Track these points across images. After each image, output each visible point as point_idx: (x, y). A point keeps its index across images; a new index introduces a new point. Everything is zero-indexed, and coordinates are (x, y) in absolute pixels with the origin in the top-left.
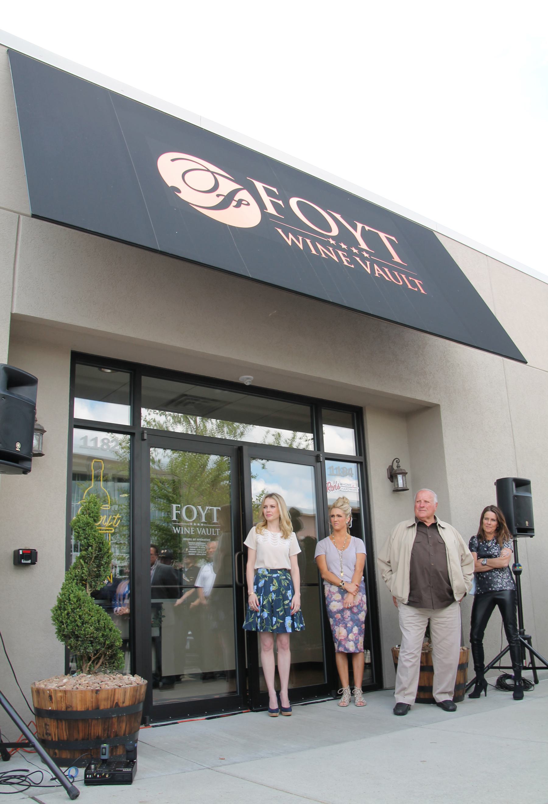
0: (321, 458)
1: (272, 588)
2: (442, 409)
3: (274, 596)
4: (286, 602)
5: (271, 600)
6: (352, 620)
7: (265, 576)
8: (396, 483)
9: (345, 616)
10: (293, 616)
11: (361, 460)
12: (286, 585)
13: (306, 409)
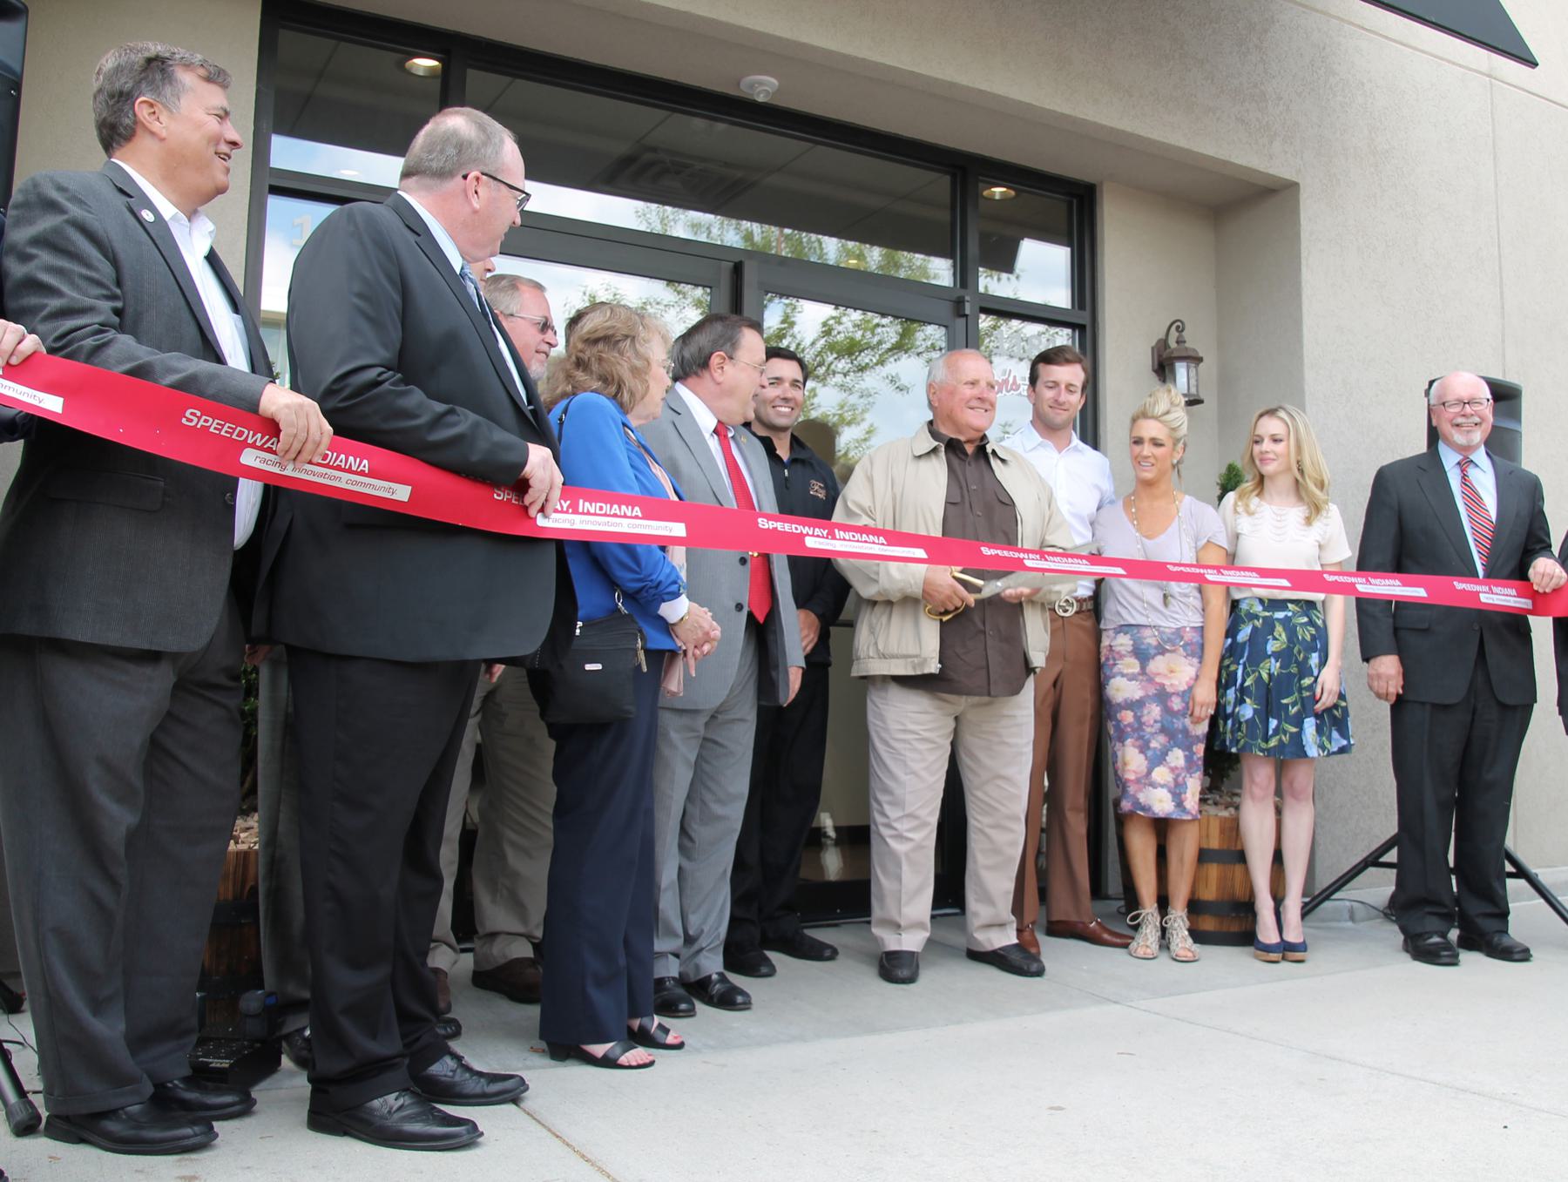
0: (967, 306)
1: (1272, 646)
2: (1304, 196)
3: (1274, 666)
4: (1307, 681)
5: (1265, 676)
6: (1163, 730)
9: (1144, 719)
11: (1083, 318)
12: (1308, 638)
13: (939, 184)
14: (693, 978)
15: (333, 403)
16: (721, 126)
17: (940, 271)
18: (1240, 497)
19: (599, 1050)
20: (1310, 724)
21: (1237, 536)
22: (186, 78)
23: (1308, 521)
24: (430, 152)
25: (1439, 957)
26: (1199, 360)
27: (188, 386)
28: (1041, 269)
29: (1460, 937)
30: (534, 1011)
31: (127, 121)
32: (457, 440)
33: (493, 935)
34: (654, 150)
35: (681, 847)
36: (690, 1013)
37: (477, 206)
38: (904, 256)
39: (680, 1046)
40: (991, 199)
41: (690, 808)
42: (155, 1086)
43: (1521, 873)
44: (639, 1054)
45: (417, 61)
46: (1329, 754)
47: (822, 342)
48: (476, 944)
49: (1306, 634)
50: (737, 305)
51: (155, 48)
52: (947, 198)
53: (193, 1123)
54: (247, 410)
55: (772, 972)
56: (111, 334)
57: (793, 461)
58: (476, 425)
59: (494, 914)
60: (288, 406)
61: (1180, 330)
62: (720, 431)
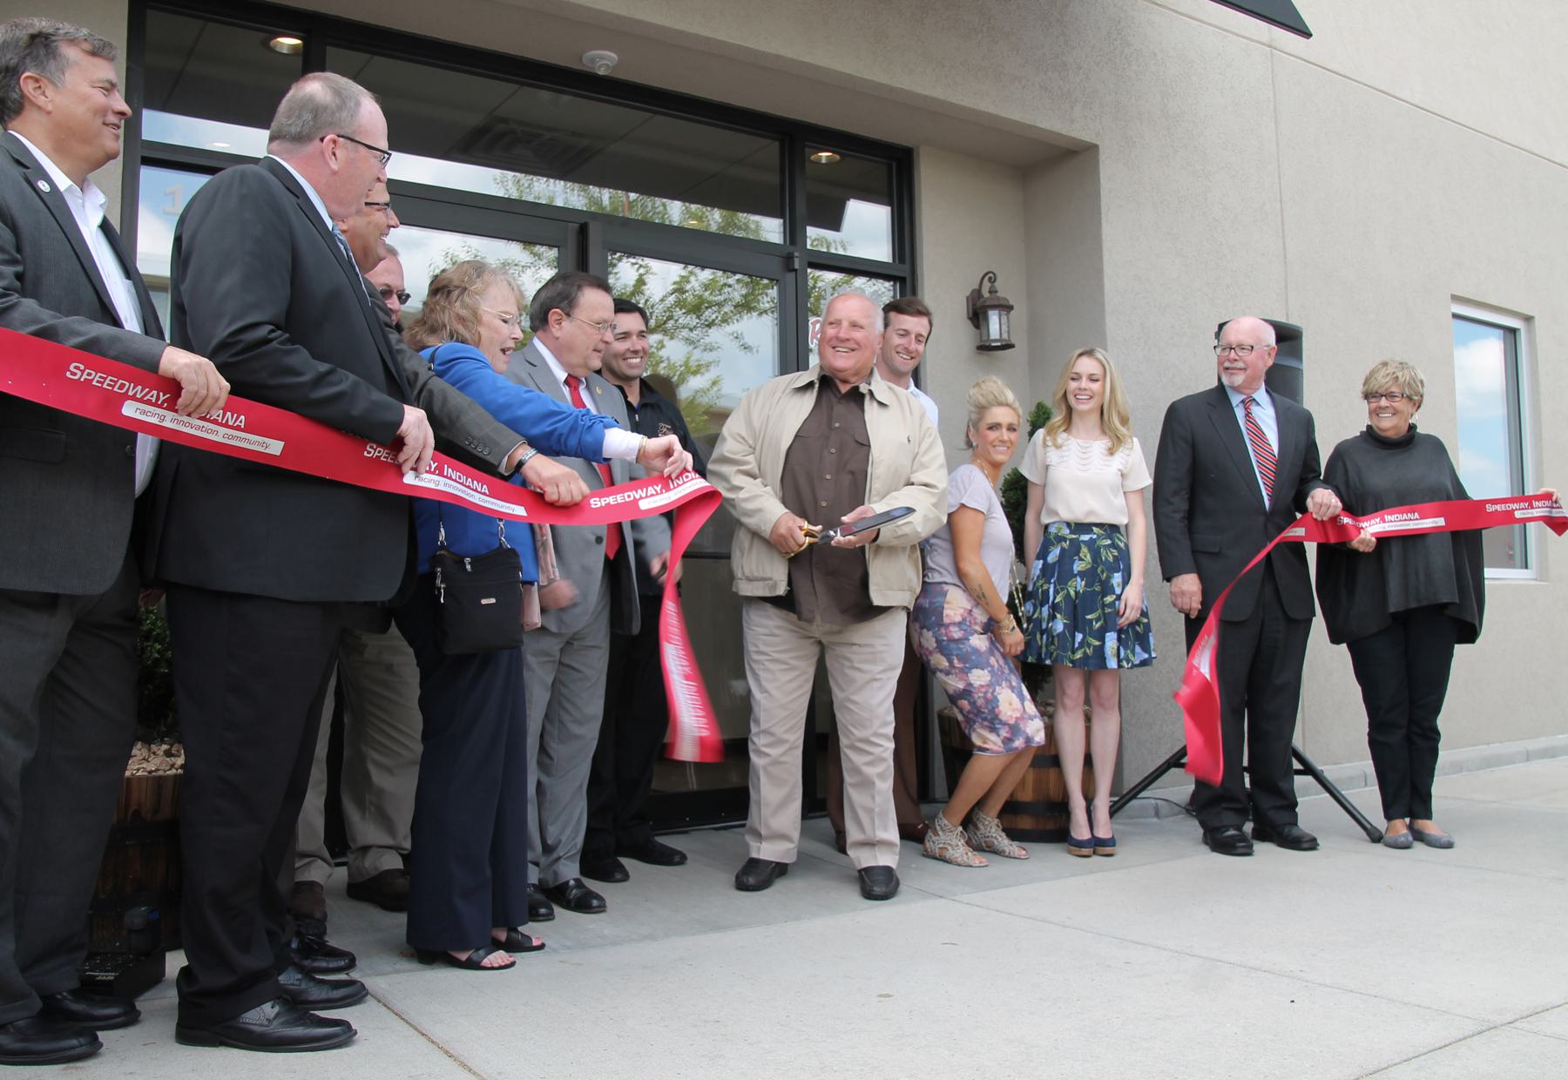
1: (1078, 567)
2: (1102, 157)
3: (1079, 585)
4: (1109, 599)
7: (1062, 539)
8: (984, 331)
10: (1120, 632)
11: (902, 273)
13: (768, 150)
14: (551, 884)
15: (223, 358)
16: (566, 98)
17: (771, 229)
18: (1048, 433)
19: (463, 956)
20: (1111, 640)
21: (1047, 467)
22: (71, 53)
23: (1111, 452)
24: (289, 117)
25: (1234, 847)
26: (1009, 308)
27: (92, 349)
28: (865, 227)
29: (1254, 830)
30: (402, 919)
31: (14, 96)
32: (340, 396)
33: (366, 849)
34: (505, 120)
35: (540, 764)
36: (550, 916)
37: (334, 166)
38: (742, 217)
39: (542, 947)
40: (818, 163)
41: (548, 727)
42: (43, 998)
43: (1308, 770)
44: (499, 957)
45: (281, 40)
46: (1134, 666)
47: (672, 299)
48: (350, 858)
49: (1109, 556)
50: (583, 263)
51: (41, 24)
52: (779, 161)
53: (77, 1034)
54: (147, 371)
55: (626, 877)
56: (15, 298)
57: (643, 405)
58: (356, 385)
59: (365, 830)
60: (187, 365)
61: (992, 281)
62: (572, 381)
